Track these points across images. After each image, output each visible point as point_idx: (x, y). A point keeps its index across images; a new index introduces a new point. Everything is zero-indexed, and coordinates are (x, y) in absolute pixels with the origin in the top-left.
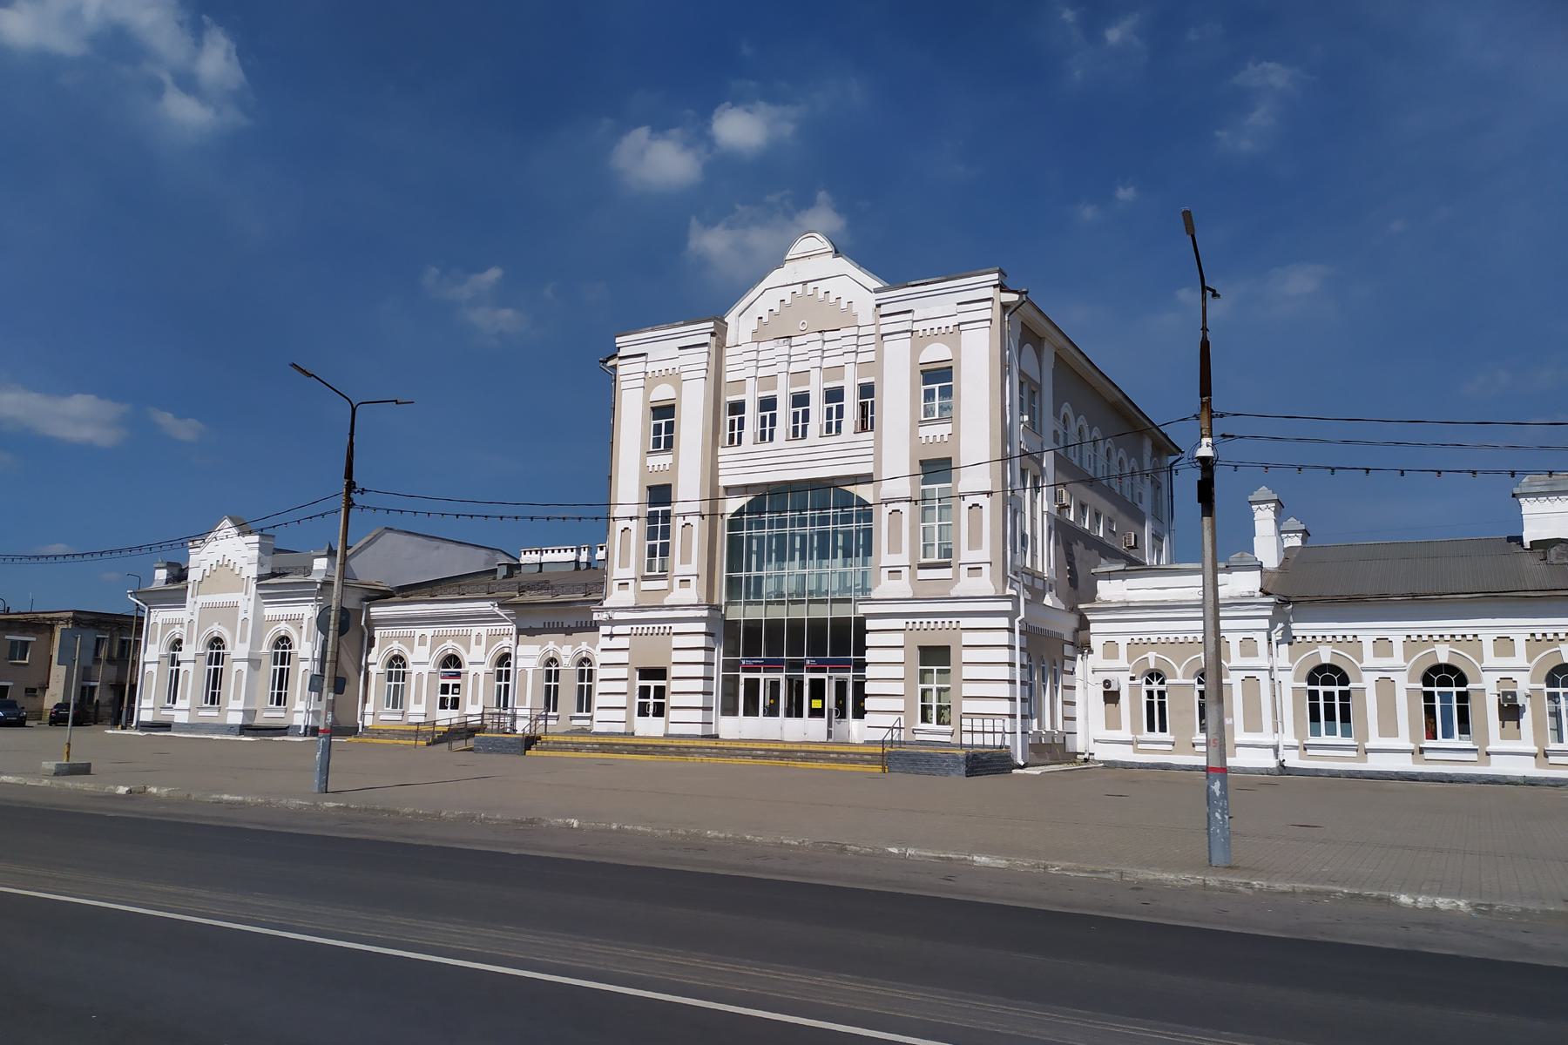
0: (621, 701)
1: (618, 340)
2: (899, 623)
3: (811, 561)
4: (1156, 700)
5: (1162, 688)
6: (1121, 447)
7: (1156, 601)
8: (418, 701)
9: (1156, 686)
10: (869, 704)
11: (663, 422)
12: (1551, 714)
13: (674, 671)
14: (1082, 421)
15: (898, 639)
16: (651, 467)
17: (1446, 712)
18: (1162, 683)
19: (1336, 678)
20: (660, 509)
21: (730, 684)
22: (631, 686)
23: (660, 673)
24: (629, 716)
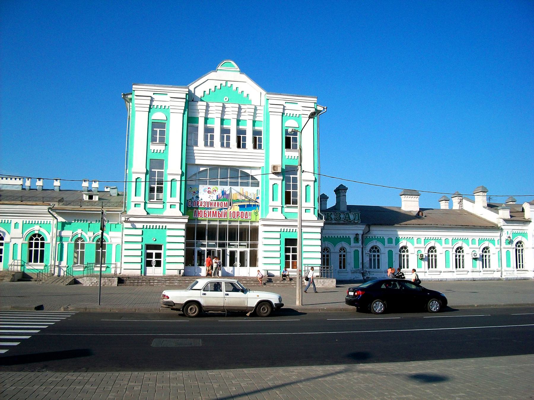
1: (134, 86)
2: (278, 229)
4: (376, 258)
7: (453, 232)
12: (129, 279)
15: (277, 235)
19: (376, 250)
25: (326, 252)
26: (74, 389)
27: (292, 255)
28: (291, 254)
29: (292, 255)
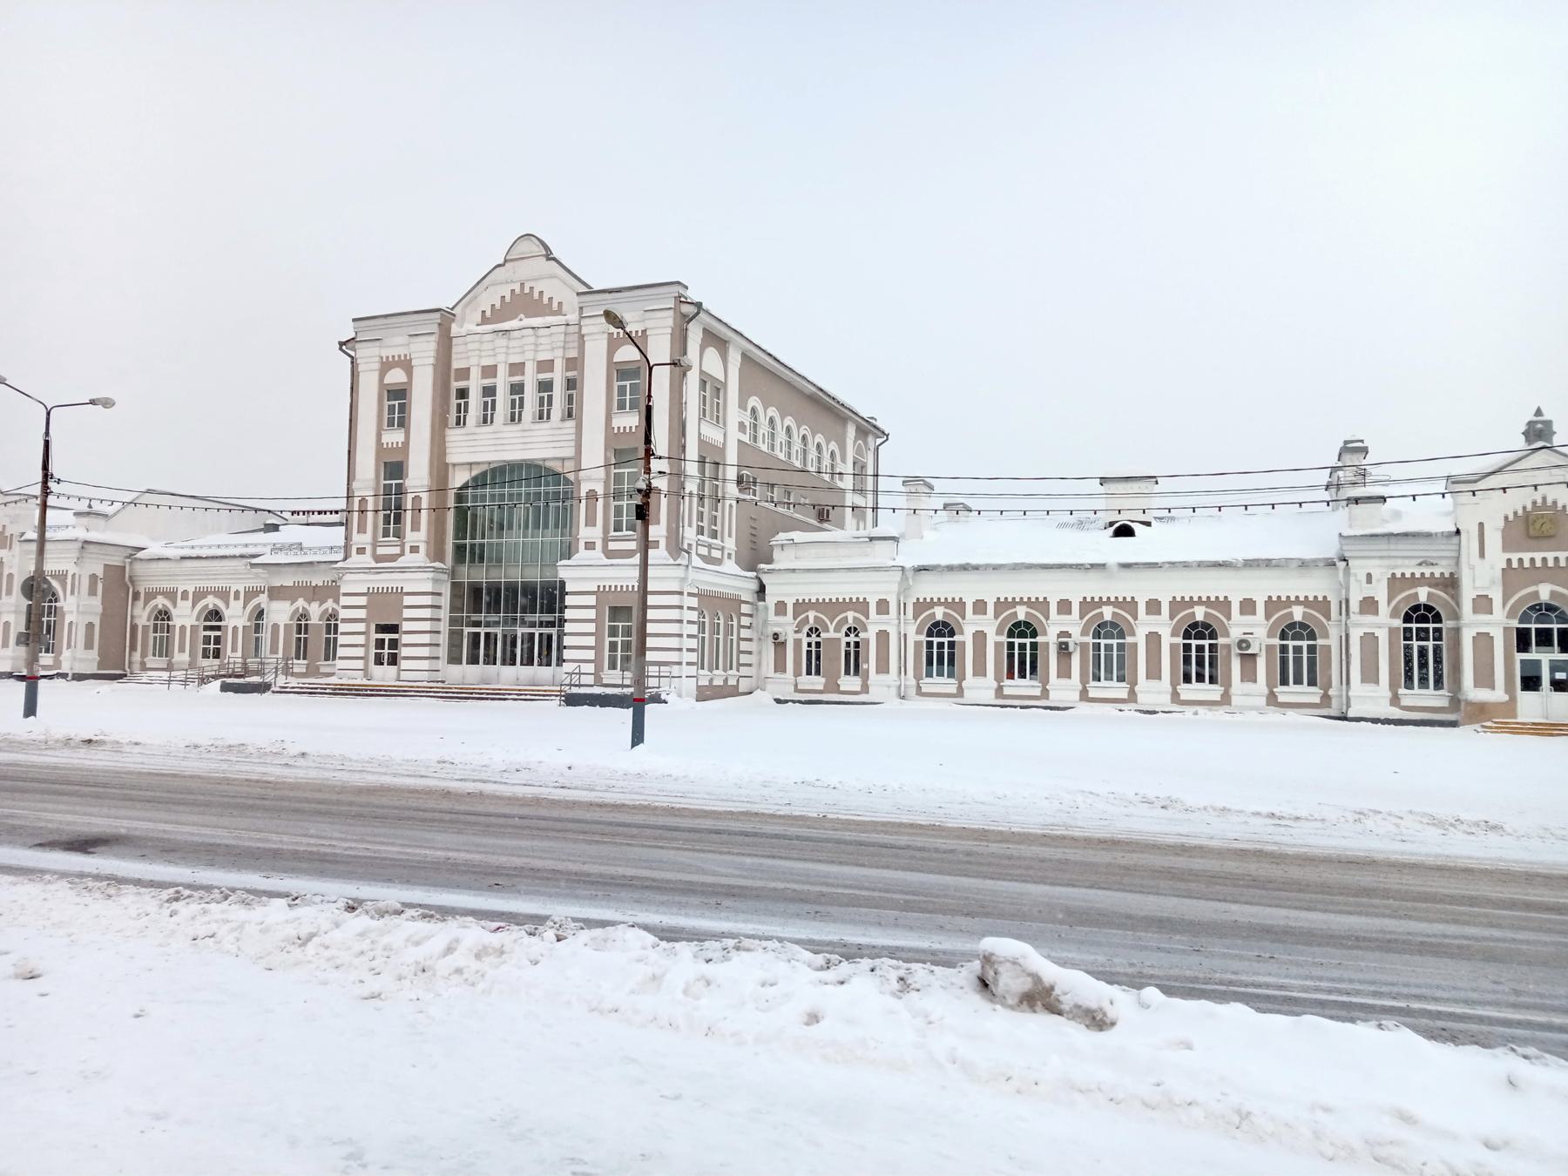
0: (360, 652)
3: (536, 531)
5: (818, 639)
6: (818, 432)
8: (182, 650)
9: (814, 639)
10: (567, 654)
11: (397, 403)
13: (406, 626)
14: (772, 411)
16: (616, 429)
17: (1109, 659)
18: (818, 636)
20: (394, 482)
21: (455, 637)
22: (368, 640)
23: (394, 629)
24: (366, 665)
25: (852, 635)
26: (751, 802)
27: (1434, 645)
28: (619, 639)
29: (1434, 645)
